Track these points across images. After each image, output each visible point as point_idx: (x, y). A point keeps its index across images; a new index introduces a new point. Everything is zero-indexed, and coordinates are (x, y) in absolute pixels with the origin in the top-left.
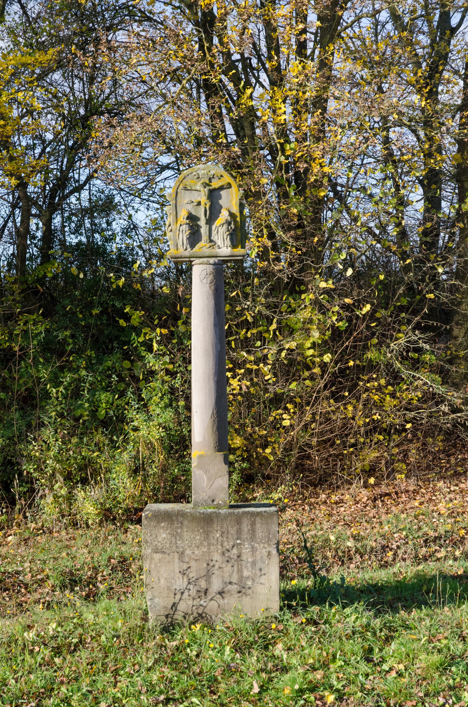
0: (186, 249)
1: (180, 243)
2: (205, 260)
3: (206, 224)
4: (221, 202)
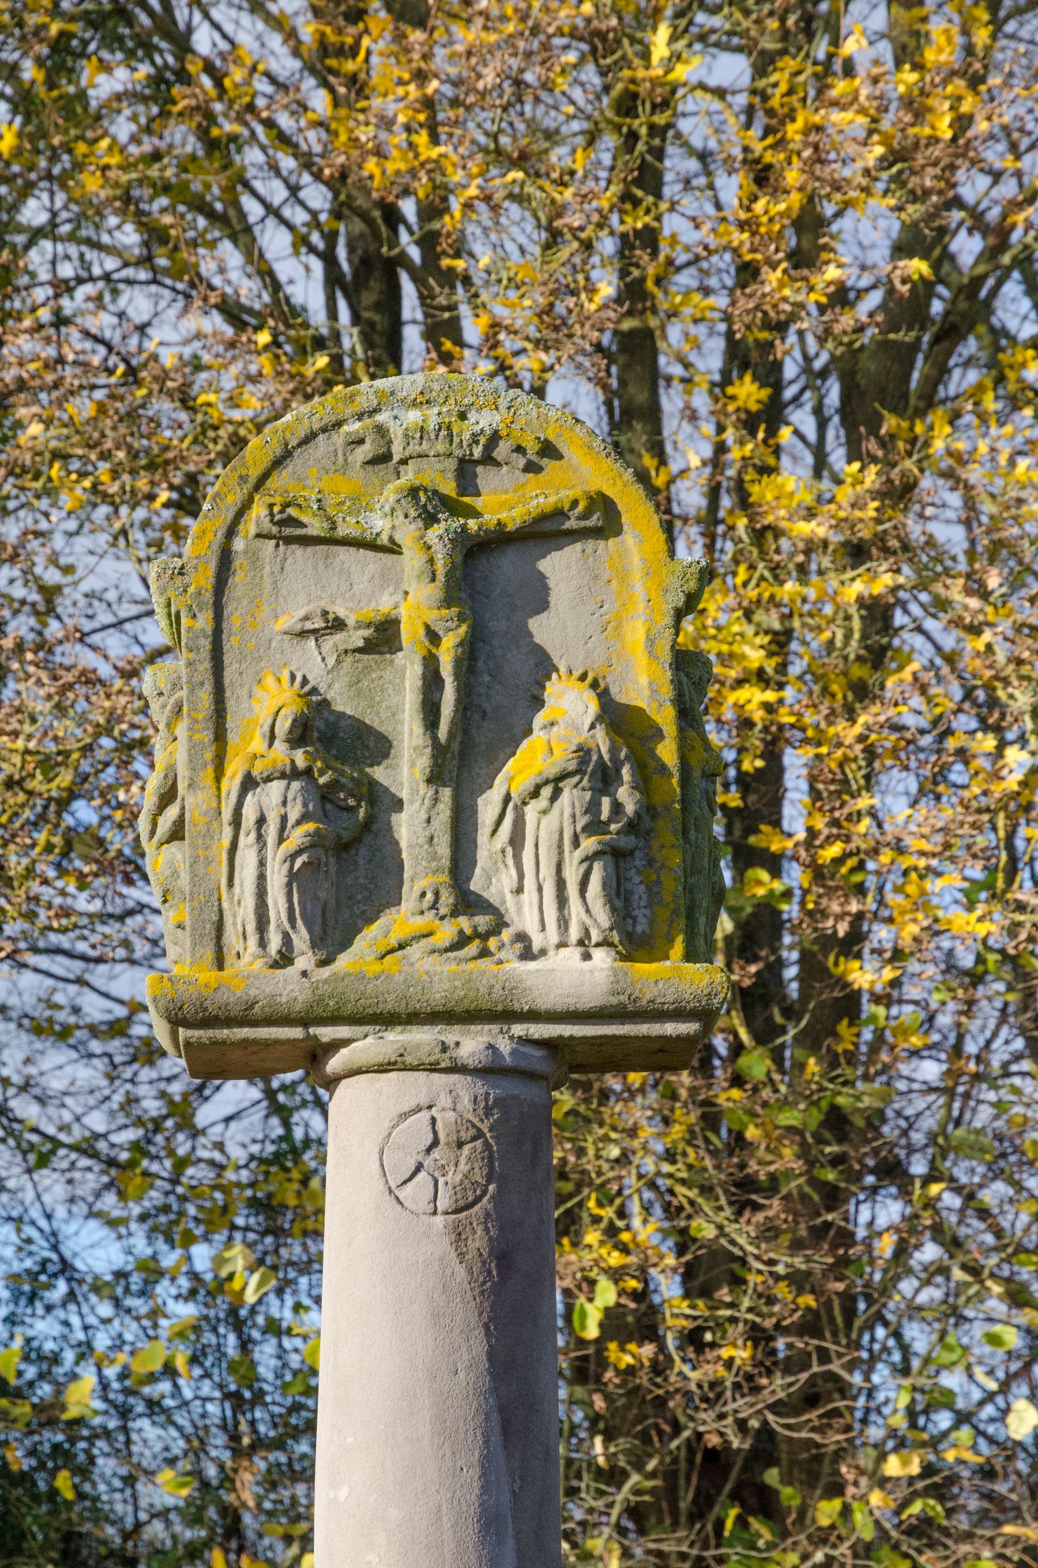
0: (285, 959)
1: (241, 913)
2: (422, 1038)
3: (435, 778)
4: (542, 629)
